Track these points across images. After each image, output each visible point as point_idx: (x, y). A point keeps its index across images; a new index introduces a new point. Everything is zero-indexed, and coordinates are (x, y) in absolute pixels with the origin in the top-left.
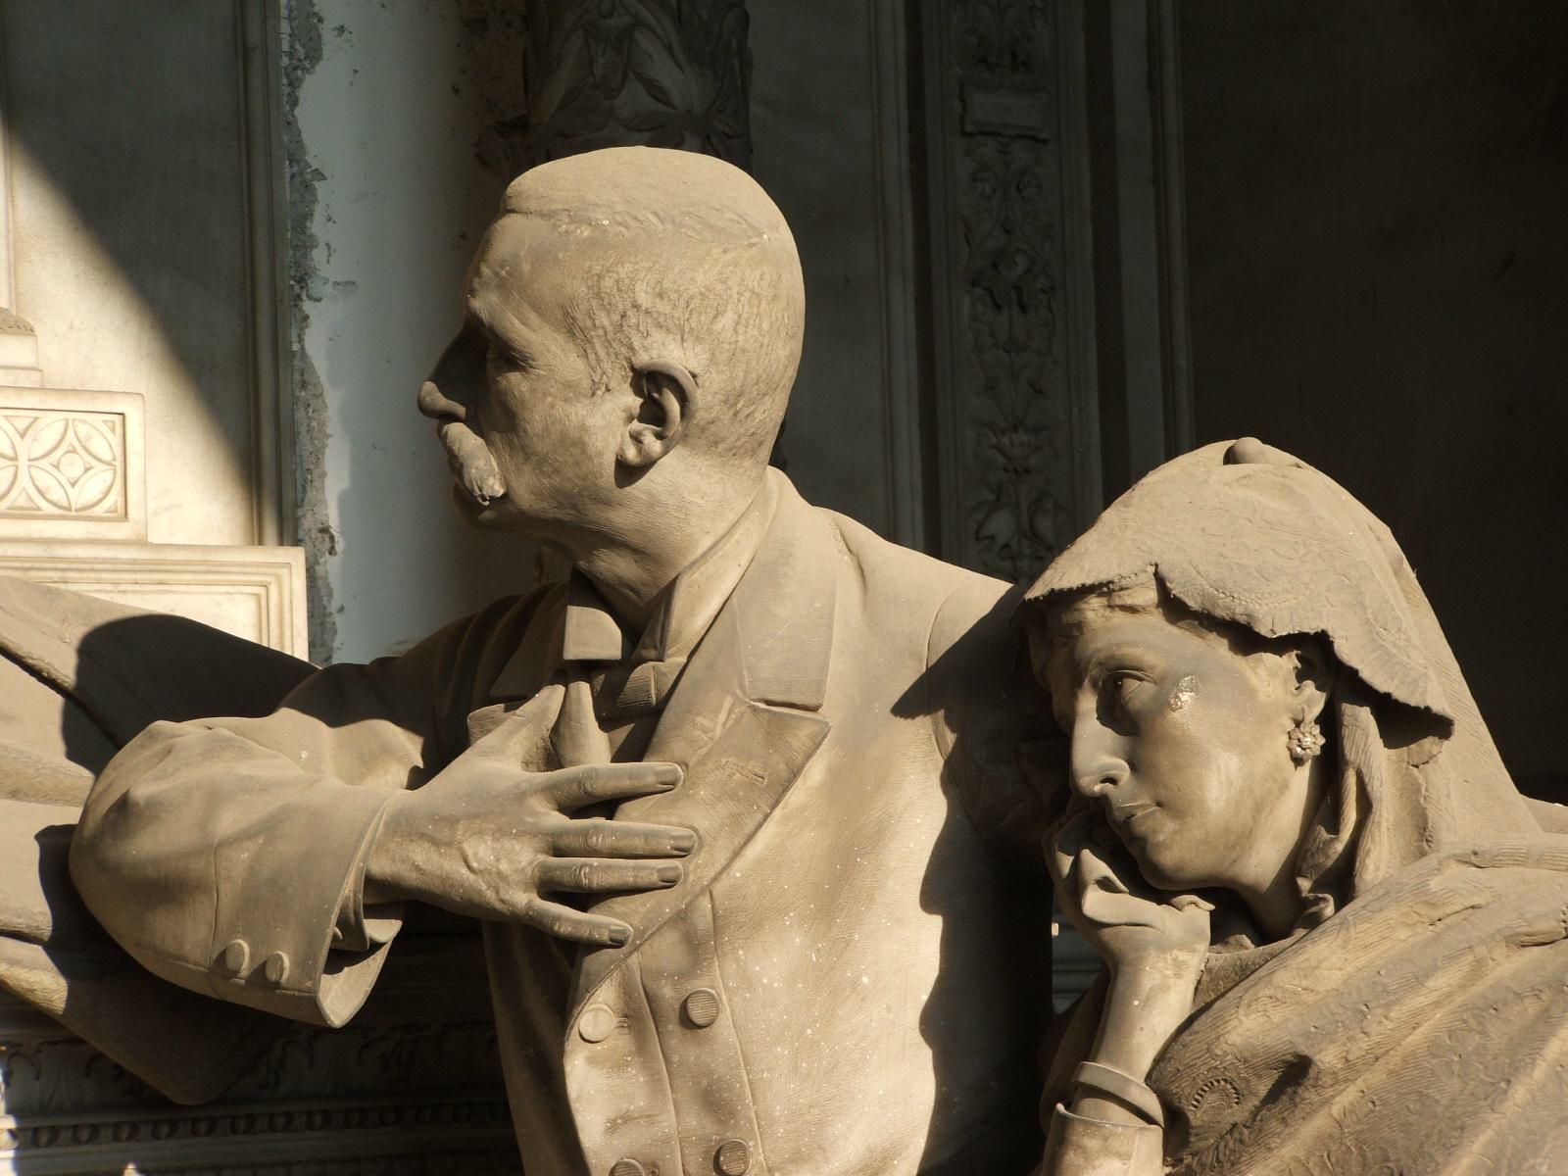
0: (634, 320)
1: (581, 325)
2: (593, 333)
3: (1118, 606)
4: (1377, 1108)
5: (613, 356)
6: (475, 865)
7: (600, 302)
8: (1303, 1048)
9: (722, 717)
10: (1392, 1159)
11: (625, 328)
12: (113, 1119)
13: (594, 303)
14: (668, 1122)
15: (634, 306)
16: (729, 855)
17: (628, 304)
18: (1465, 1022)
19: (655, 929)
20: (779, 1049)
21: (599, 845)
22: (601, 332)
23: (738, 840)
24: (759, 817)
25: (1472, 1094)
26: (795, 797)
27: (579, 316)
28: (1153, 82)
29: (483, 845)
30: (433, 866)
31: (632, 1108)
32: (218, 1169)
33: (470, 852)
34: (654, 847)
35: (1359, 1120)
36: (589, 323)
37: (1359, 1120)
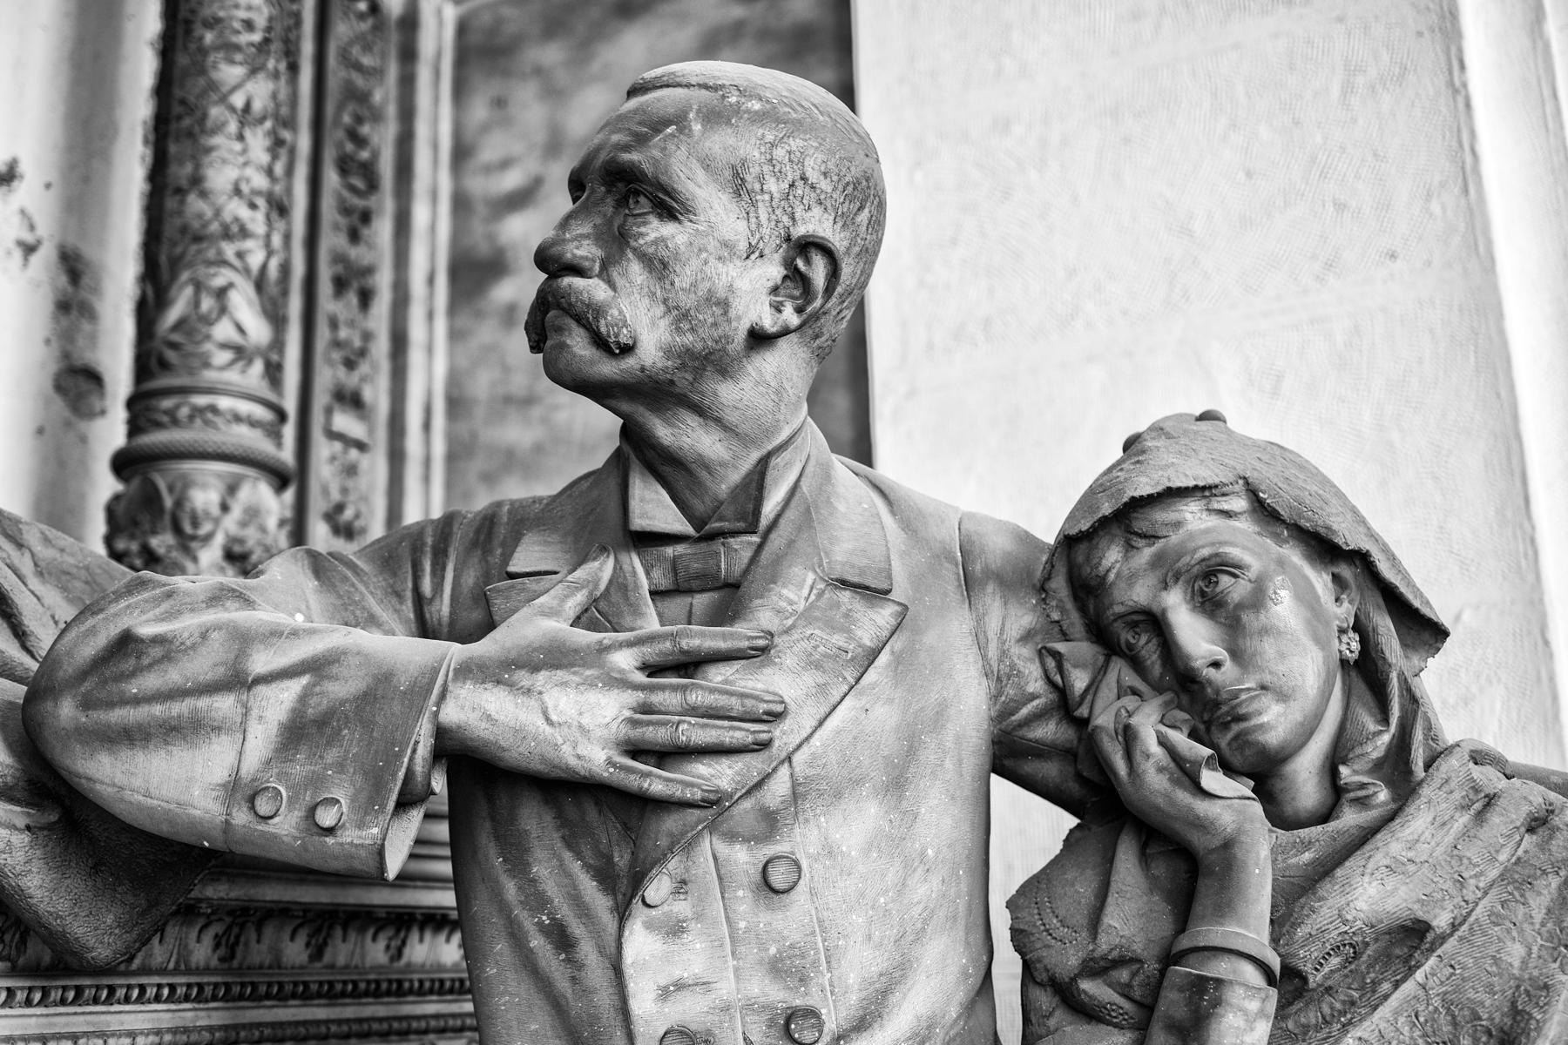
0: (800, 192)
1: (749, 187)
2: (758, 197)
3: (1215, 510)
4: (1458, 972)
5: (773, 223)
6: (554, 718)
7: (771, 168)
8: (1421, 913)
9: (805, 592)
10: (1484, 1017)
11: (791, 197)
12: (28, 984)
13: (766, 168)
14: (726, 988)
15: (802, 179)
16: (814, 723)
17: (798, 174)
18: (1510, 894)
19: (744, 791)
20: (854, 917)
21: (699, 703)
22: (767, 197)
23: (824, 710)
24: (845, 688)
25: (1540, 957)
26: (871, 676)
27: (748, 178)
28: (427, 426)
29: (565, 698)
30: (506, 717)
31: (686, 975)
32: (43, 1039)
33: (550, 704)
34: (1042, 683)
35: (1442, 982)
36: (757, 186)
37: (1442, 982)
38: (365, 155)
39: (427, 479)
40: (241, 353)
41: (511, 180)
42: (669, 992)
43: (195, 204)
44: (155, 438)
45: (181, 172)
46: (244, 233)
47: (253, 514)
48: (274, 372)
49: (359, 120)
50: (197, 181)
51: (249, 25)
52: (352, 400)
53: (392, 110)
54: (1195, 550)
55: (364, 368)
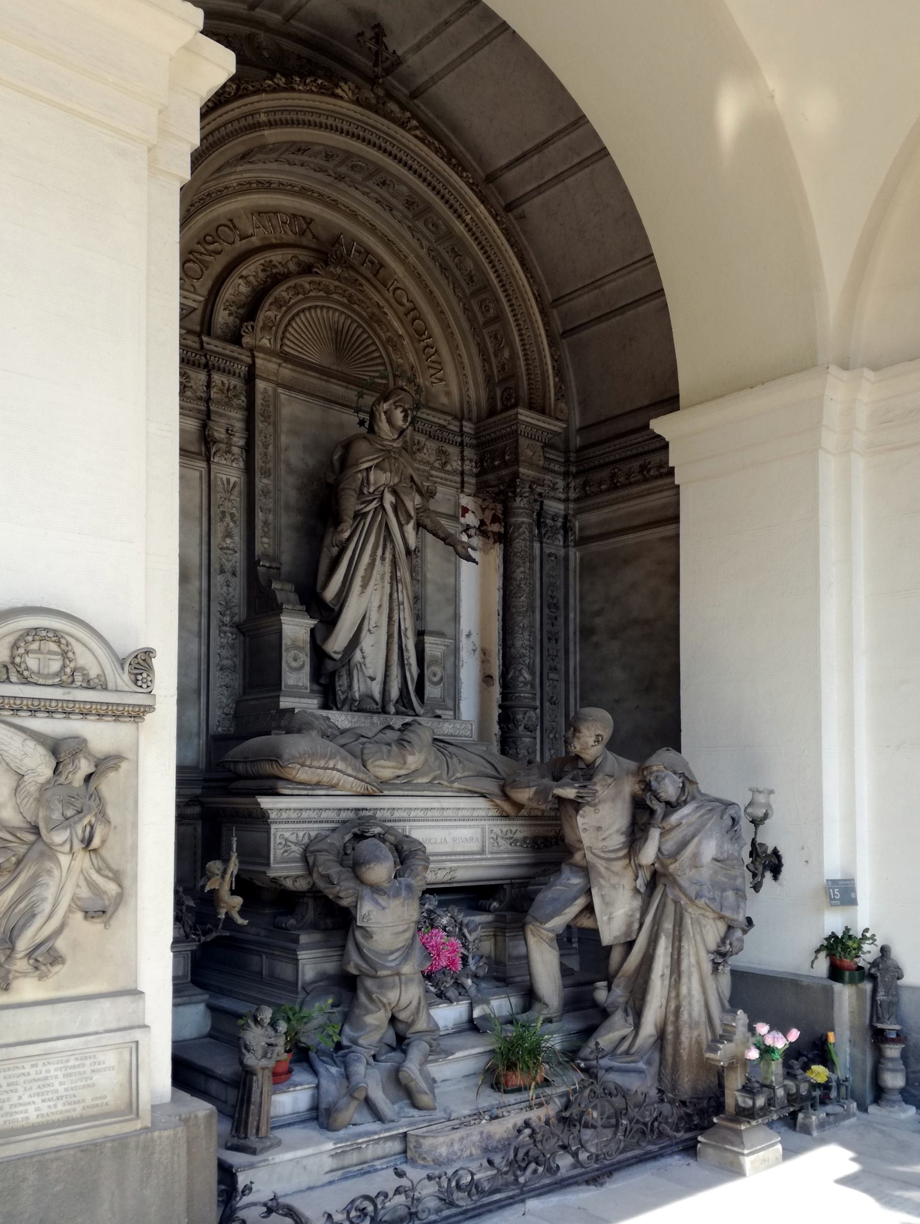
38: (555, 601)
39: (575, 688)
40: (525, 684)
41: (596, 607)
42: (583, 824)
43: (513, 650)
44: (506, 703)
45: (509, 643)
46: (524, 656)
47: (530, 718)
48: (533, 686)
49: (553, 592)
50: (513, 645)
51: (523, 606)
52: (554, 669)
53: (562, 586)
54: (521, 825)
55: (557, 660)
